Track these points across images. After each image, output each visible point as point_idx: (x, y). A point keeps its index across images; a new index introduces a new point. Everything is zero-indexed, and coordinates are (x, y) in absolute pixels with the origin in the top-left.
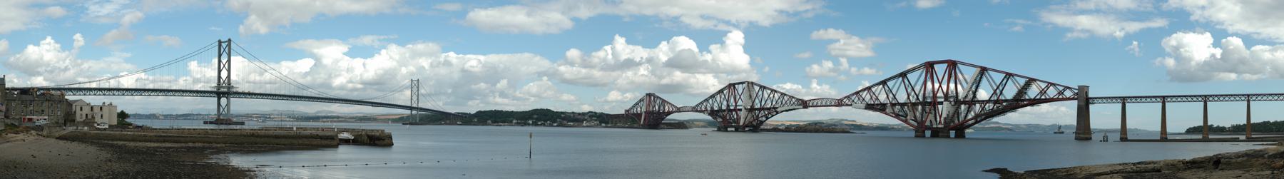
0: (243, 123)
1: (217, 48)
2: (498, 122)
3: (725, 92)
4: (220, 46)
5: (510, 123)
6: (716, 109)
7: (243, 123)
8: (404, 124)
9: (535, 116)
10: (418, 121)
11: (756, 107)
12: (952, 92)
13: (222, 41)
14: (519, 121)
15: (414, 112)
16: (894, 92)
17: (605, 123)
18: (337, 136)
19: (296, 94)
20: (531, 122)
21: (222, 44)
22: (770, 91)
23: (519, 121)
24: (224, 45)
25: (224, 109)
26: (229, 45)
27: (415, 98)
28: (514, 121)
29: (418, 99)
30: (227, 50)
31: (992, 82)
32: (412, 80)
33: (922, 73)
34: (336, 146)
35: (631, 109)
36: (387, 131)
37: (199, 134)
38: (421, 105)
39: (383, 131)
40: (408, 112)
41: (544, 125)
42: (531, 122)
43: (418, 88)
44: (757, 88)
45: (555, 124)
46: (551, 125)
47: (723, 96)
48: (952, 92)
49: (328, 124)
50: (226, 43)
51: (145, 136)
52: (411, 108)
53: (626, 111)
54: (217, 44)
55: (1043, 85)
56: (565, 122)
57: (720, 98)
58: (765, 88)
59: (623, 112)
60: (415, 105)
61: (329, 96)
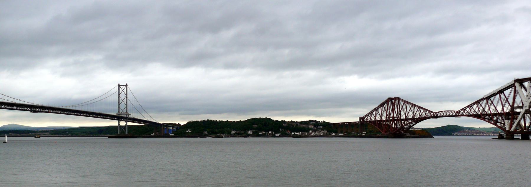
2: (86, 129)
3: (385, 105)
5: (228, 134)
6: (379, 119)
9: (255, 126)
10: (127, 133)
11: (410, 117)
14: (238, 132)
15: (123, 123)
17: (336, 132)
20: (251, 133)
22: (418, 108)
23: (238, 132)
28: (233, 132)
29: (119, 105)
32: (119, 85)
33: (511, 92)
35: (367, 115)
41: (264, 136)
42: (251, 133)
44: (402, 103)
45: (278, 135)
46: (273, 136)
47: (383, 109)
53: (361, 118)
55: (410, 110)
56: (289, 132)
57: (381, 110)
58: (408, 103)
59: (357, 120)
61: (11, 101)
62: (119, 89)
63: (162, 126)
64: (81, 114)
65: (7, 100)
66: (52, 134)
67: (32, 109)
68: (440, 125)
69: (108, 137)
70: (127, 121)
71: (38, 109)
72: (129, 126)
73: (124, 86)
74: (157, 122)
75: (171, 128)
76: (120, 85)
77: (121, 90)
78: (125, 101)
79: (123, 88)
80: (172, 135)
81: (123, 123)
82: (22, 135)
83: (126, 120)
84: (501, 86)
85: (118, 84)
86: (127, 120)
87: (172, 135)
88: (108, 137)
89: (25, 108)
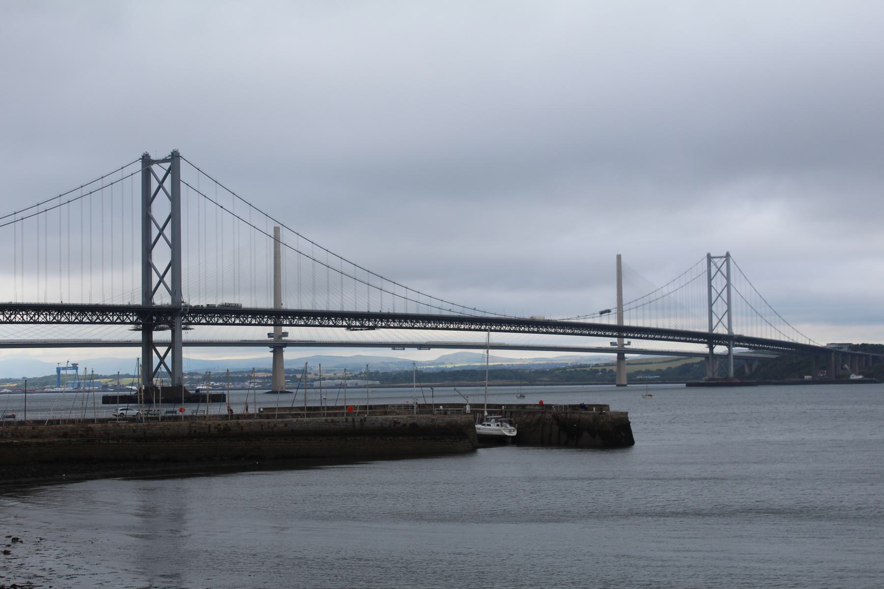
0: (219, 399)
1: (139, 177)
4: (147, 173)
5: (842, 379)
7: (219, 399)
8: (689, 385)
12: (286, 334)
13: (153, 157)
15: (720, 349)
16: (121, 296)
18: (471, 426)
19: (385, 310)
21: (155, 167)
24: (159, 171)
25: (162, 359)
26: (174, 171)
27: (720, 308)
30: (167, 184)
31: (306, 529)
32: (709, 258)
34: (471, 450)
36: (616, 406)
37: (65, 435)
38: (737, 331)
39: (602, 408)
40: (702, 348)
43: (728, 278)
48: (629, 343)
49: (444, 396)
50: (167, 165)
51: (284, 411)
52: (711, 339)
54: (139, 166)
60: (721, 330)
62: (709, 266)
63: (833, 354)
64: (688, 339)
65: (450, 310)
66: (567, 381)
67: (512, 326)
68: (460, 364)
69: (685, 385)
70: (731, 344)
71: (515, 327)
72: (736, 357)
73: (721, 257)
74: (816, 345)
75: (441, 407)
76: (712, 255)
77: (714, 270)
78: (724, 295)
79: (719, 262)
80: (861, 377)
81: (720, 349)
82: (500, 382)
83: (729, 343)
84: (541, 402)
85: (706, 255)
86: (731, 342)
87: (861, 377)
88: (685, 385)
89: (506, 326)
